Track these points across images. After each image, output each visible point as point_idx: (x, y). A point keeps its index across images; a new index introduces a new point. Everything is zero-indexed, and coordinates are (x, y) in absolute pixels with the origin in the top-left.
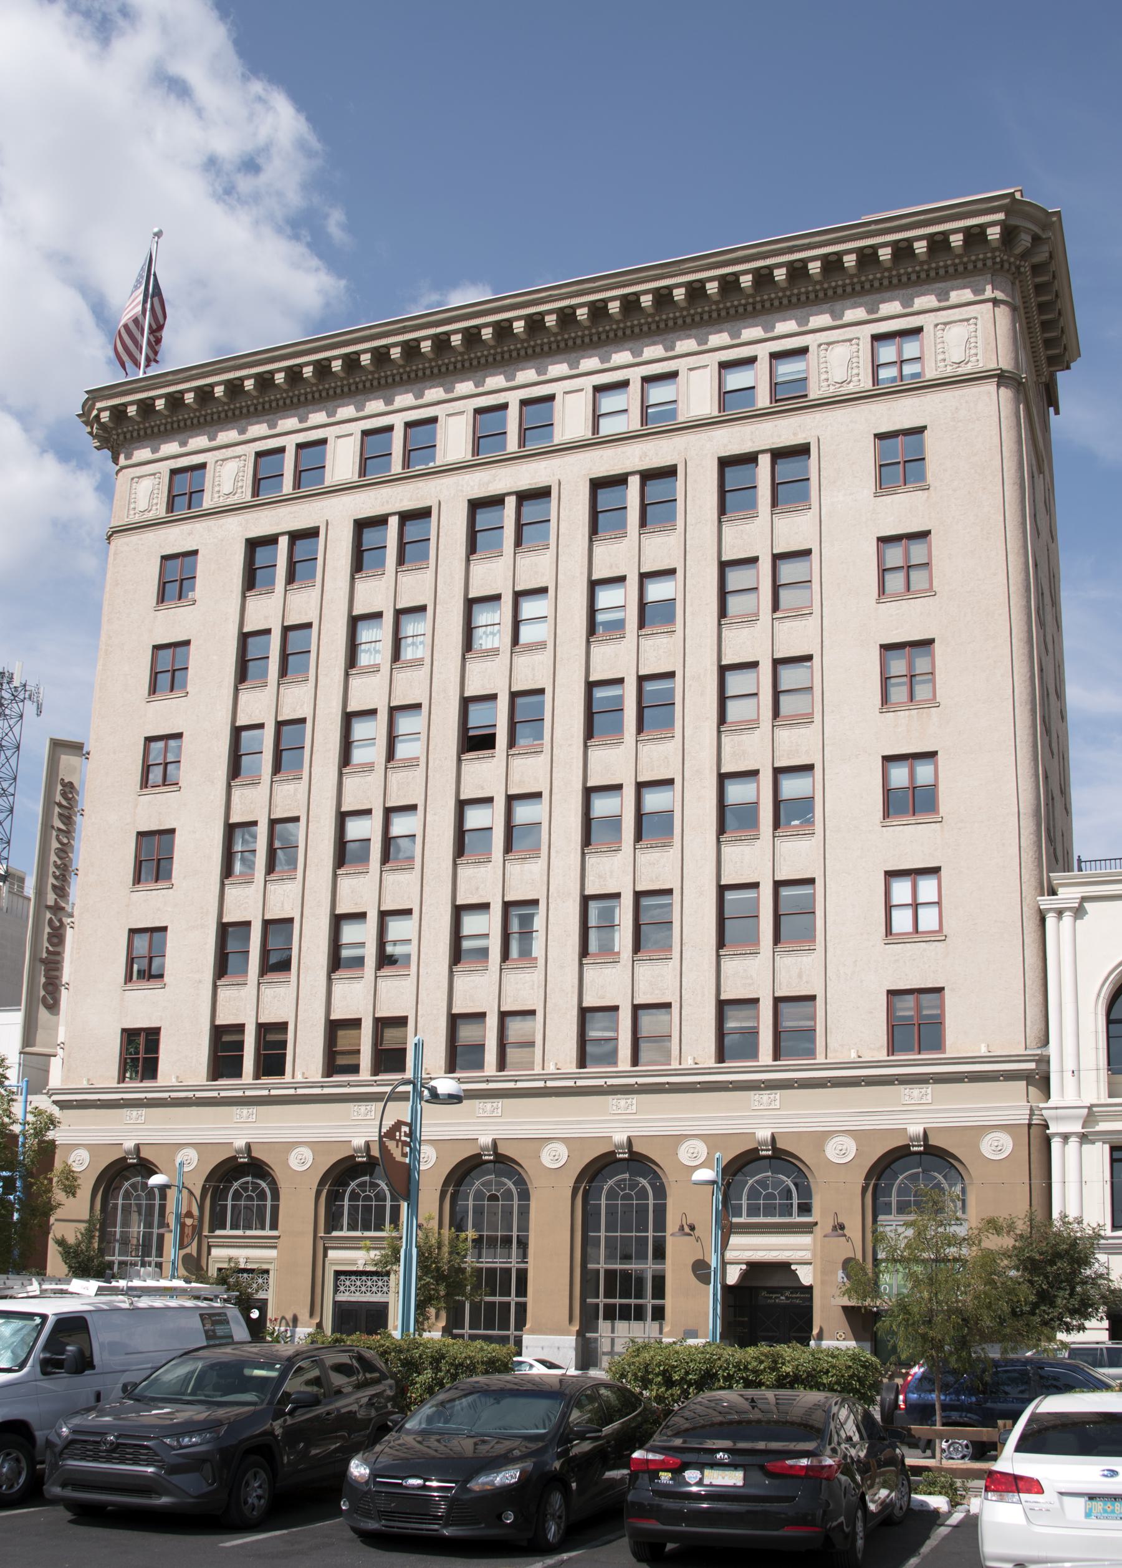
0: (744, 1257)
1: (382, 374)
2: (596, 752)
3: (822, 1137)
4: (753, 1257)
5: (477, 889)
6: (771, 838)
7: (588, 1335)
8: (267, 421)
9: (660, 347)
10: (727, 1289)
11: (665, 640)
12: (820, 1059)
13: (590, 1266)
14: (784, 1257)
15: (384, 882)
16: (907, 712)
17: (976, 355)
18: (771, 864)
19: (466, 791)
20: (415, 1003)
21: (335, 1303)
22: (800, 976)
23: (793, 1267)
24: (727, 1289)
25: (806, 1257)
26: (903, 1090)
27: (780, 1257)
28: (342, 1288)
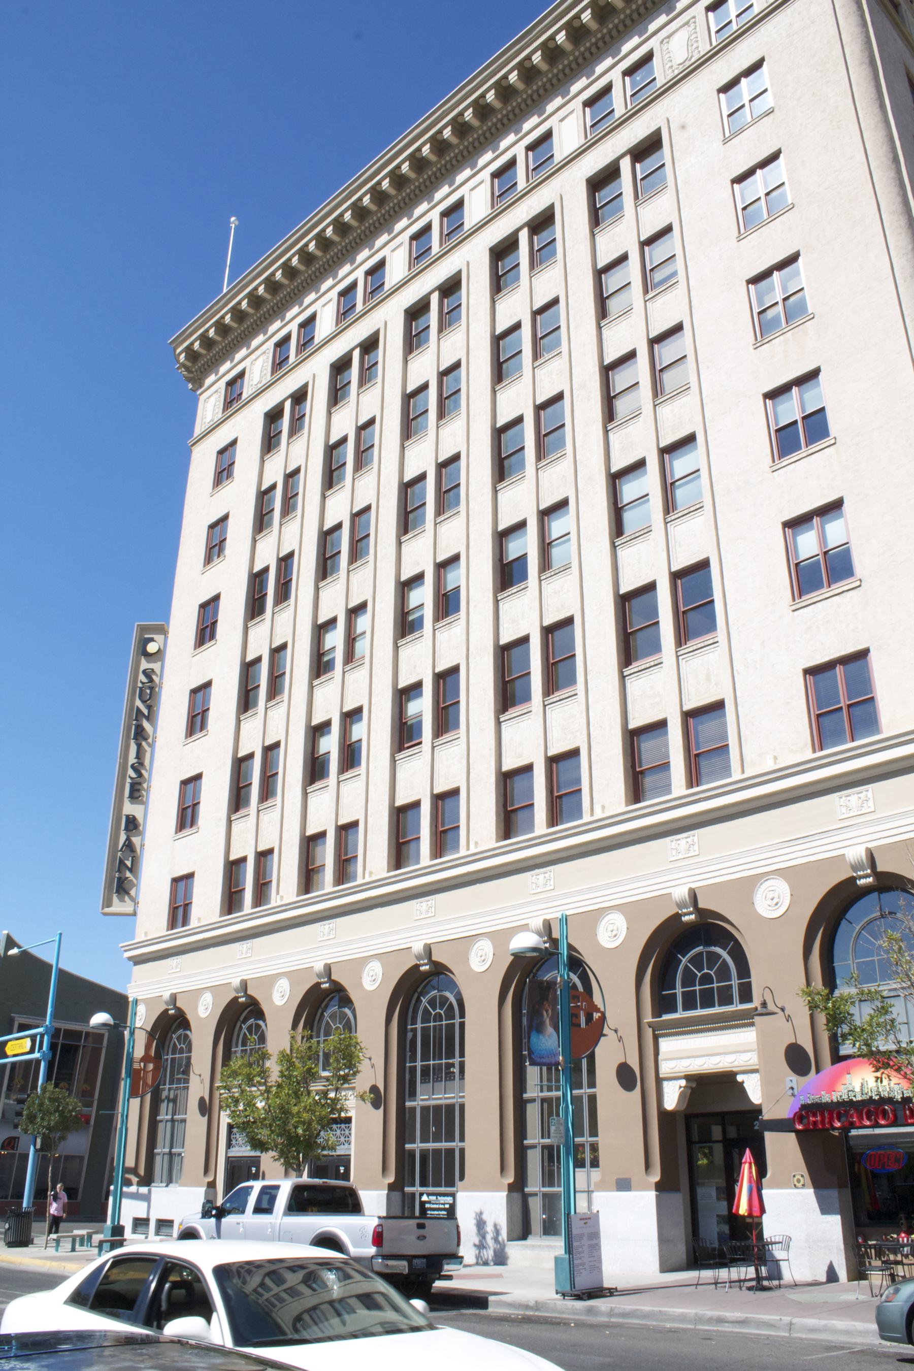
0: (682, 1069)
1: (545, 80)
2: (506, 494)
3: (749, 884)
4: (691, 1068)
5: (415, 667)
6: (662, 525)
7: (408, 1189)
8: (426, 200)
9: (584, 78)
10: (665, 1116)
11: (556, 364)
12: (736, 775)
13: (408, 1104)
14: (726, 1065)
15: (346, 683)
16: (781, 337)
17: (697, 48)
18: (665, 554)
19: (406, 571)
20: (364, 802)
21: (228, 1159)
22: (708, 679)
23: (740, 1078)
24: (665, 1117)
25: (751, 1062)
26: (837, 798)
27: (721, 1065)
28: (234, 1142)
